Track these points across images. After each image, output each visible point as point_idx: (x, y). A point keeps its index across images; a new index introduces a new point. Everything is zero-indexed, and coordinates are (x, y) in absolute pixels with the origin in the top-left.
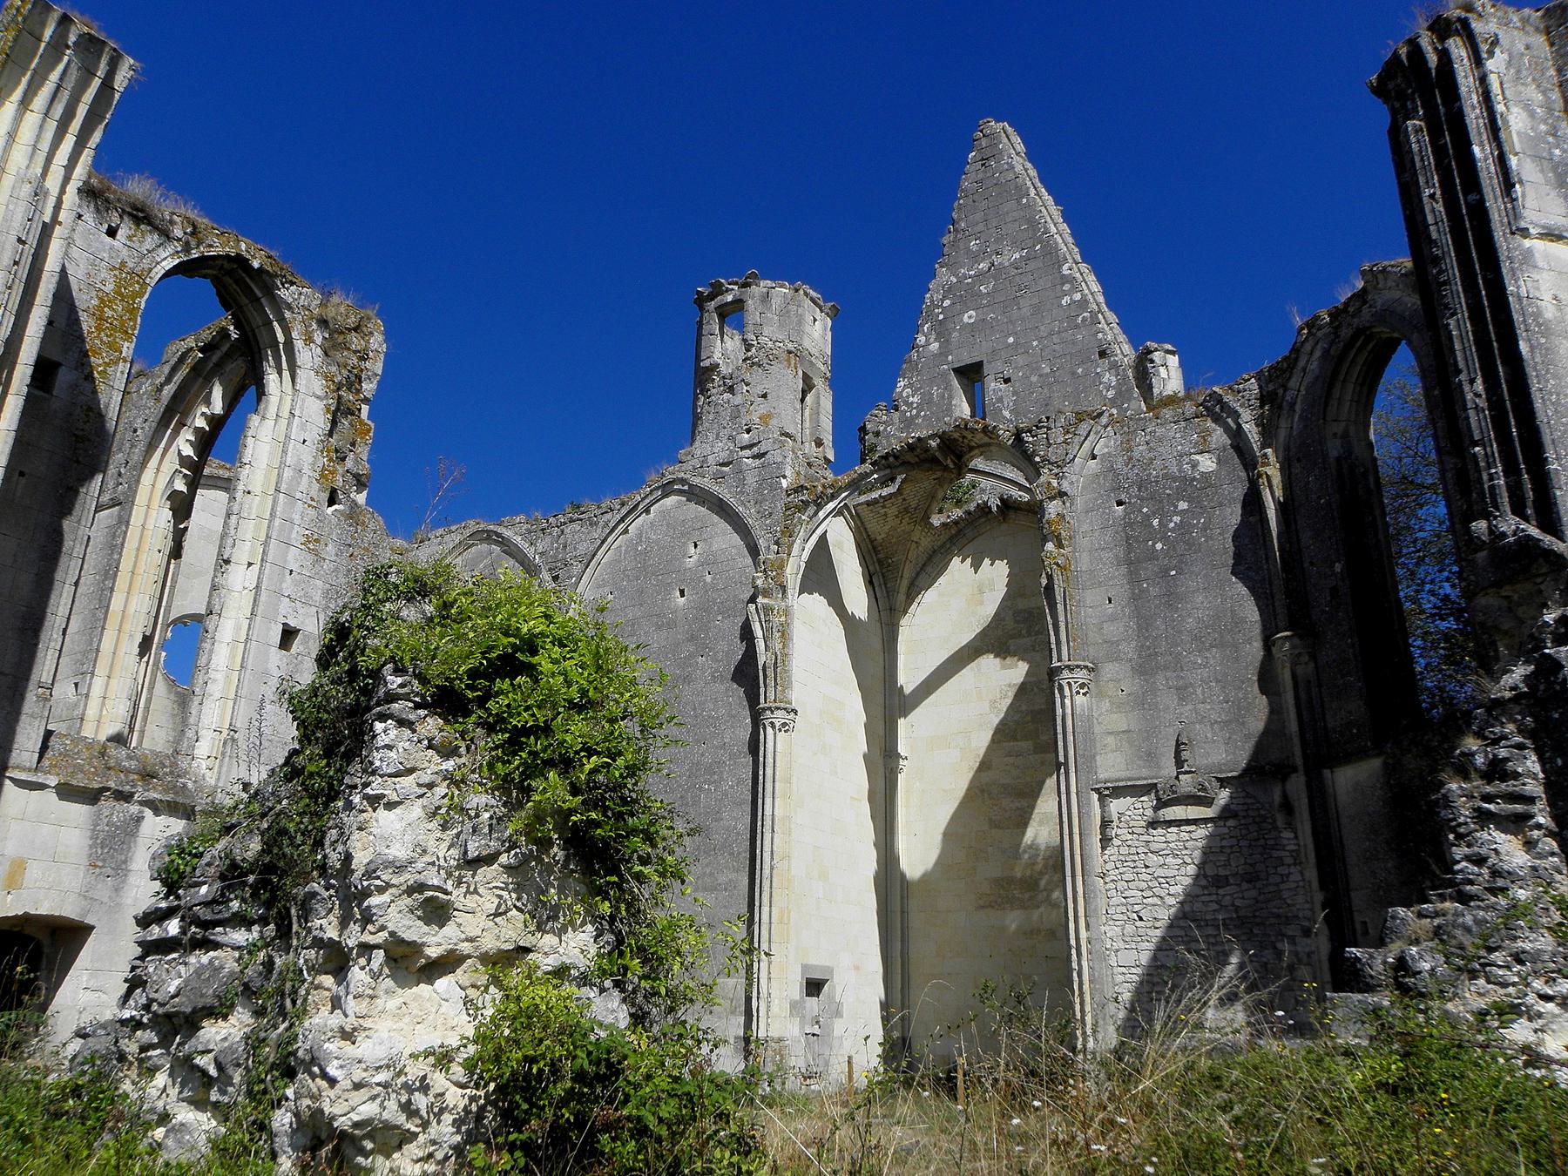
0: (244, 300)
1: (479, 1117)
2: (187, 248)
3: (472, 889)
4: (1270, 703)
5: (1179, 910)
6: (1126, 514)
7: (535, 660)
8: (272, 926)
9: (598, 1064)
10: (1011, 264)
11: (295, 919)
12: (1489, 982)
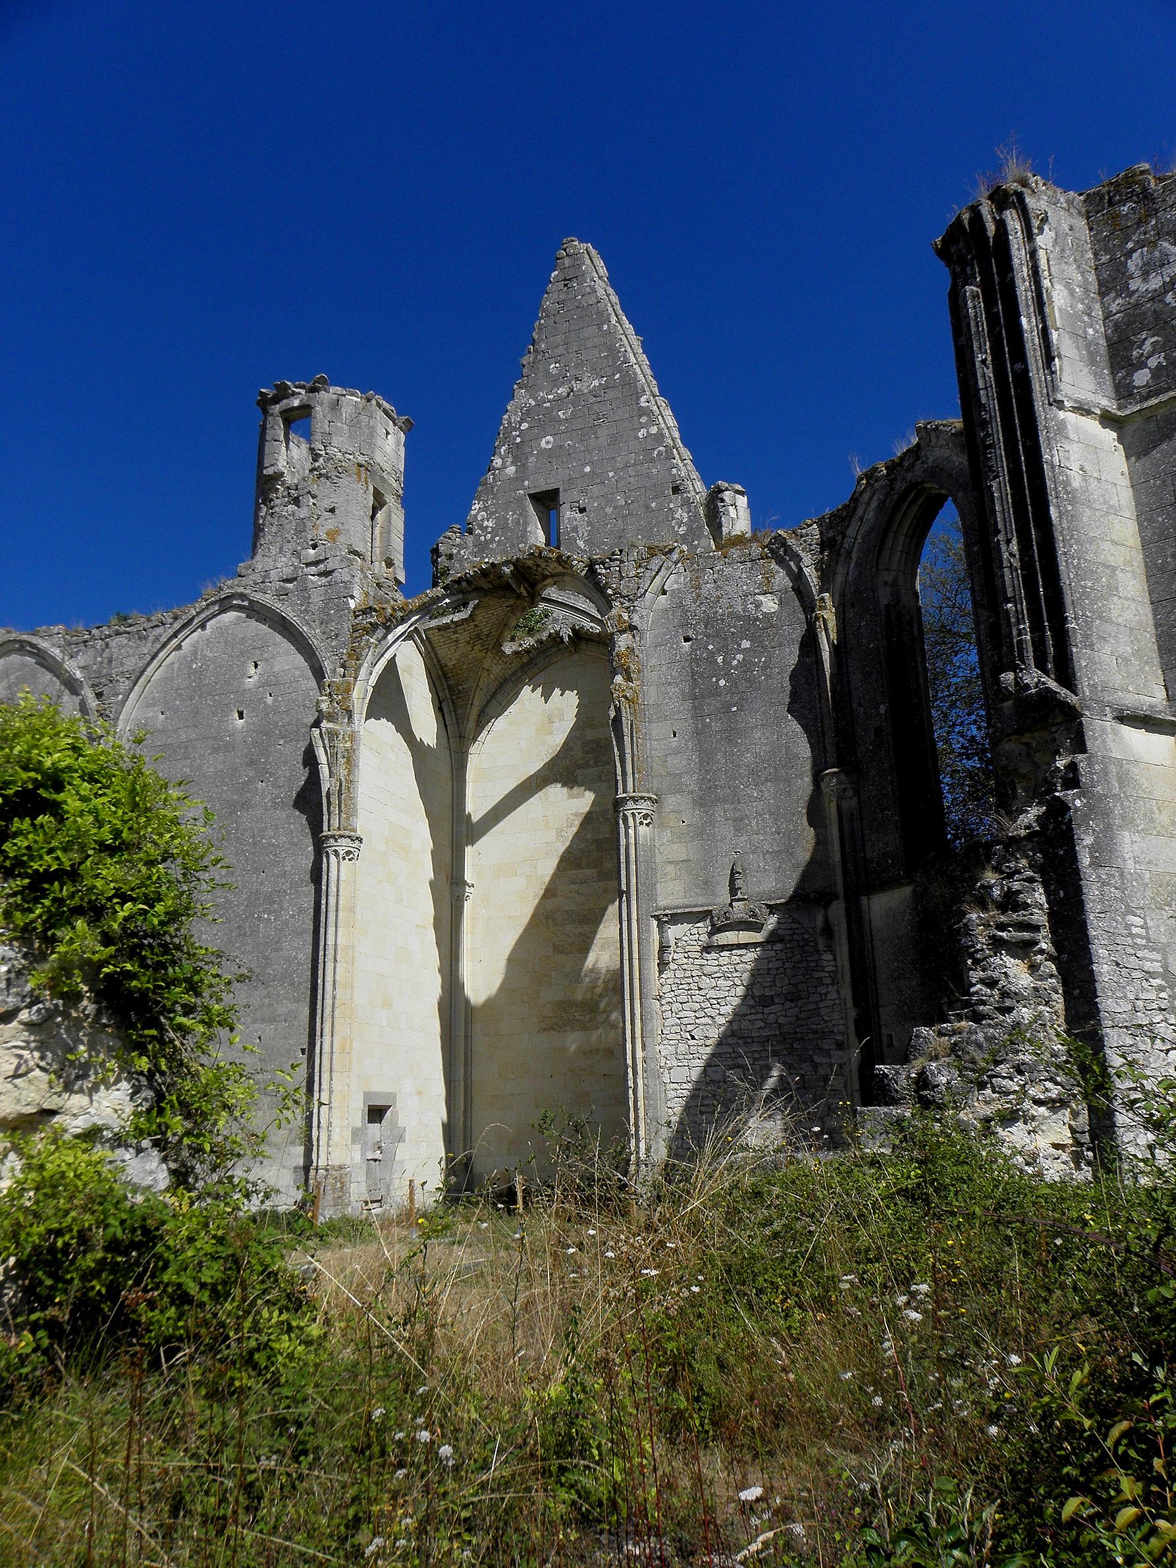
4: (817, 835)
5: (727, 1028)
6: (693, 650)
7: (61, 797)
9: (134, 1230)
10: (590, 392)
12: (994, 1092)
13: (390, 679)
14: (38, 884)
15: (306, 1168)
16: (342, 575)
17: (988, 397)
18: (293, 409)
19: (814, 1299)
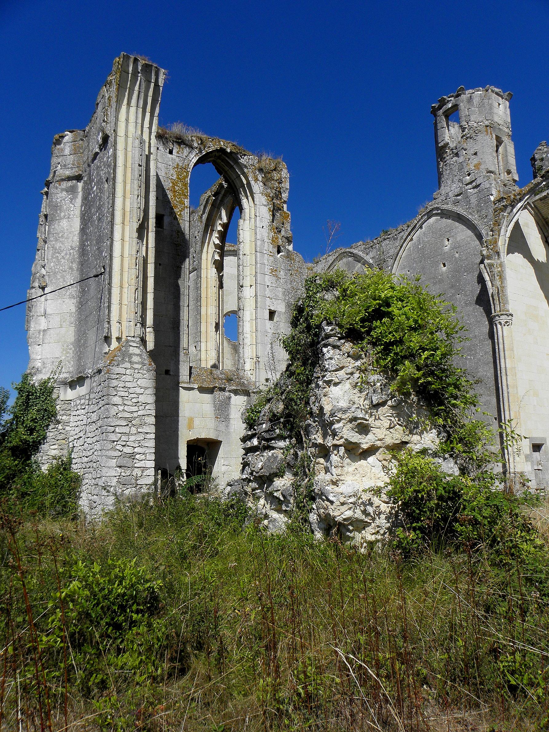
0: (227, 168)
1: (397, 515)
2: (200, 151)
3: (377, 418)
7: (390, 309)
8: (294, 439)
9: (449, 493)
11: (303, 436)
13: (517, 233)
14: (387, 348)
16: (485, 185)
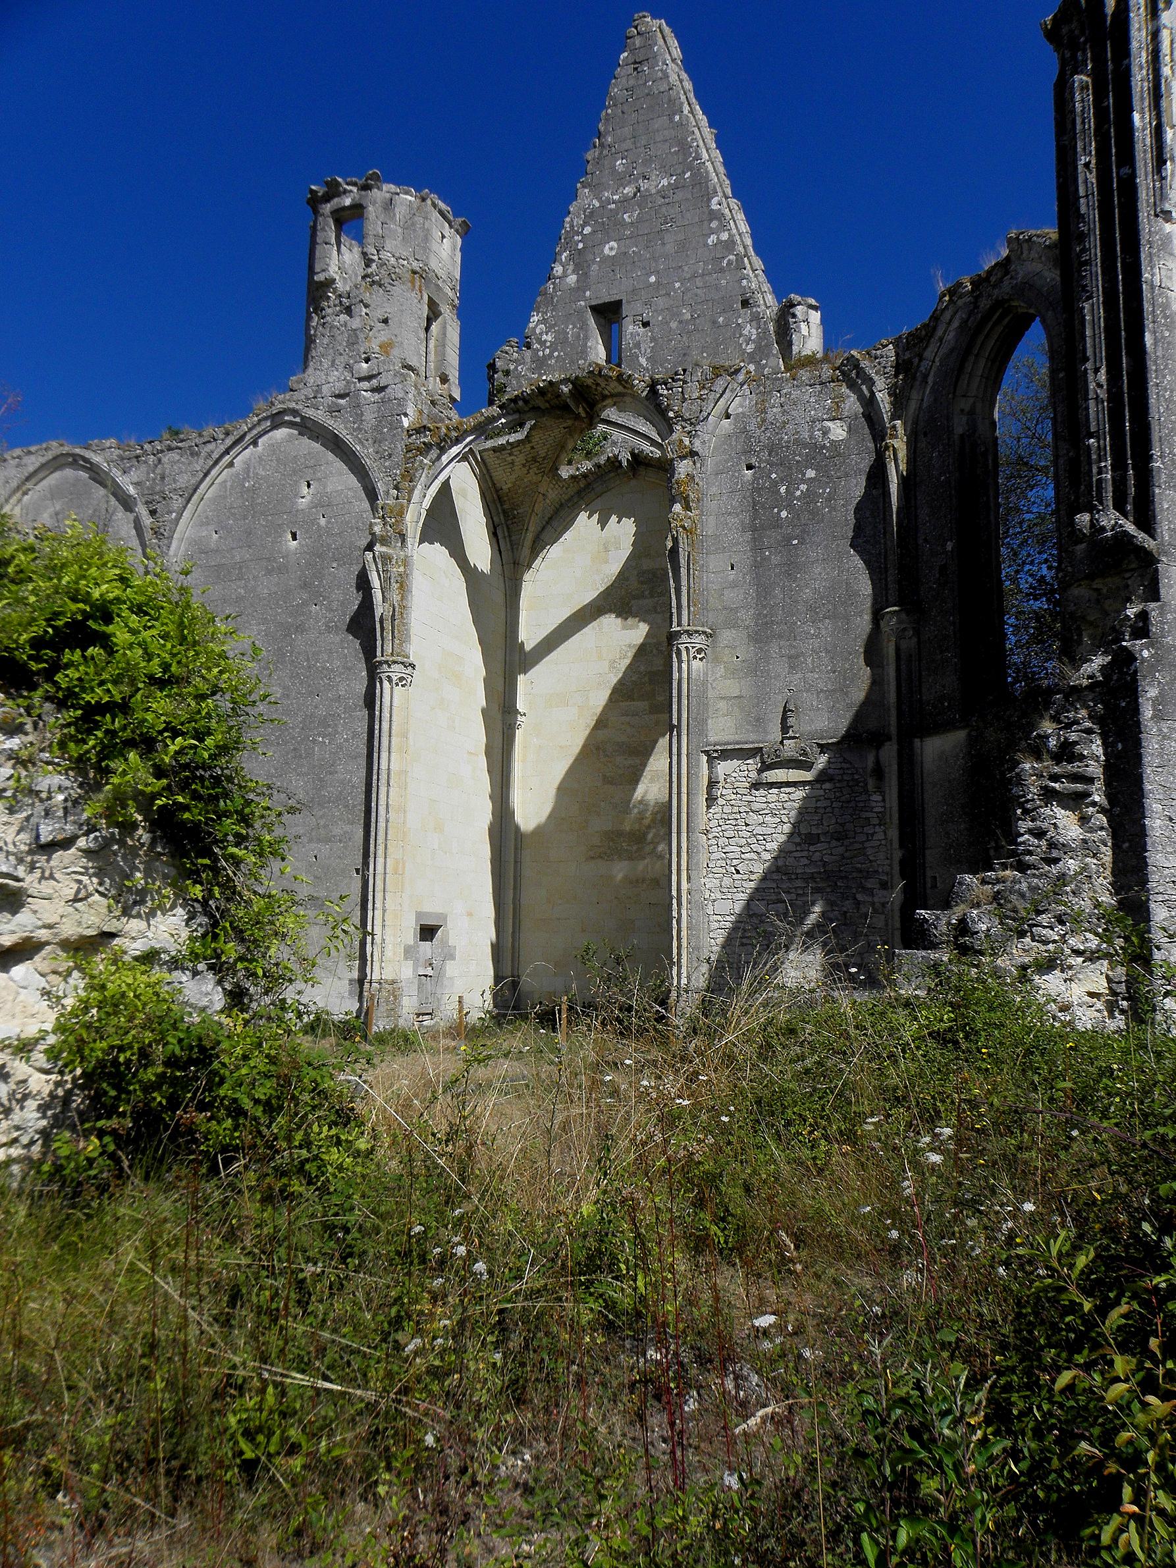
3: (47, 874)
4: (873, 674)
6: (755, 478)
7: (110, 629)
10: (659, 192)
12: (1033, 941)
13: (444, 503)
14: (91, 715)
15: (361, 981)
16: (395, 391)
17: (1088, 207)
18: (344, 208)
19: (841, 1133)
